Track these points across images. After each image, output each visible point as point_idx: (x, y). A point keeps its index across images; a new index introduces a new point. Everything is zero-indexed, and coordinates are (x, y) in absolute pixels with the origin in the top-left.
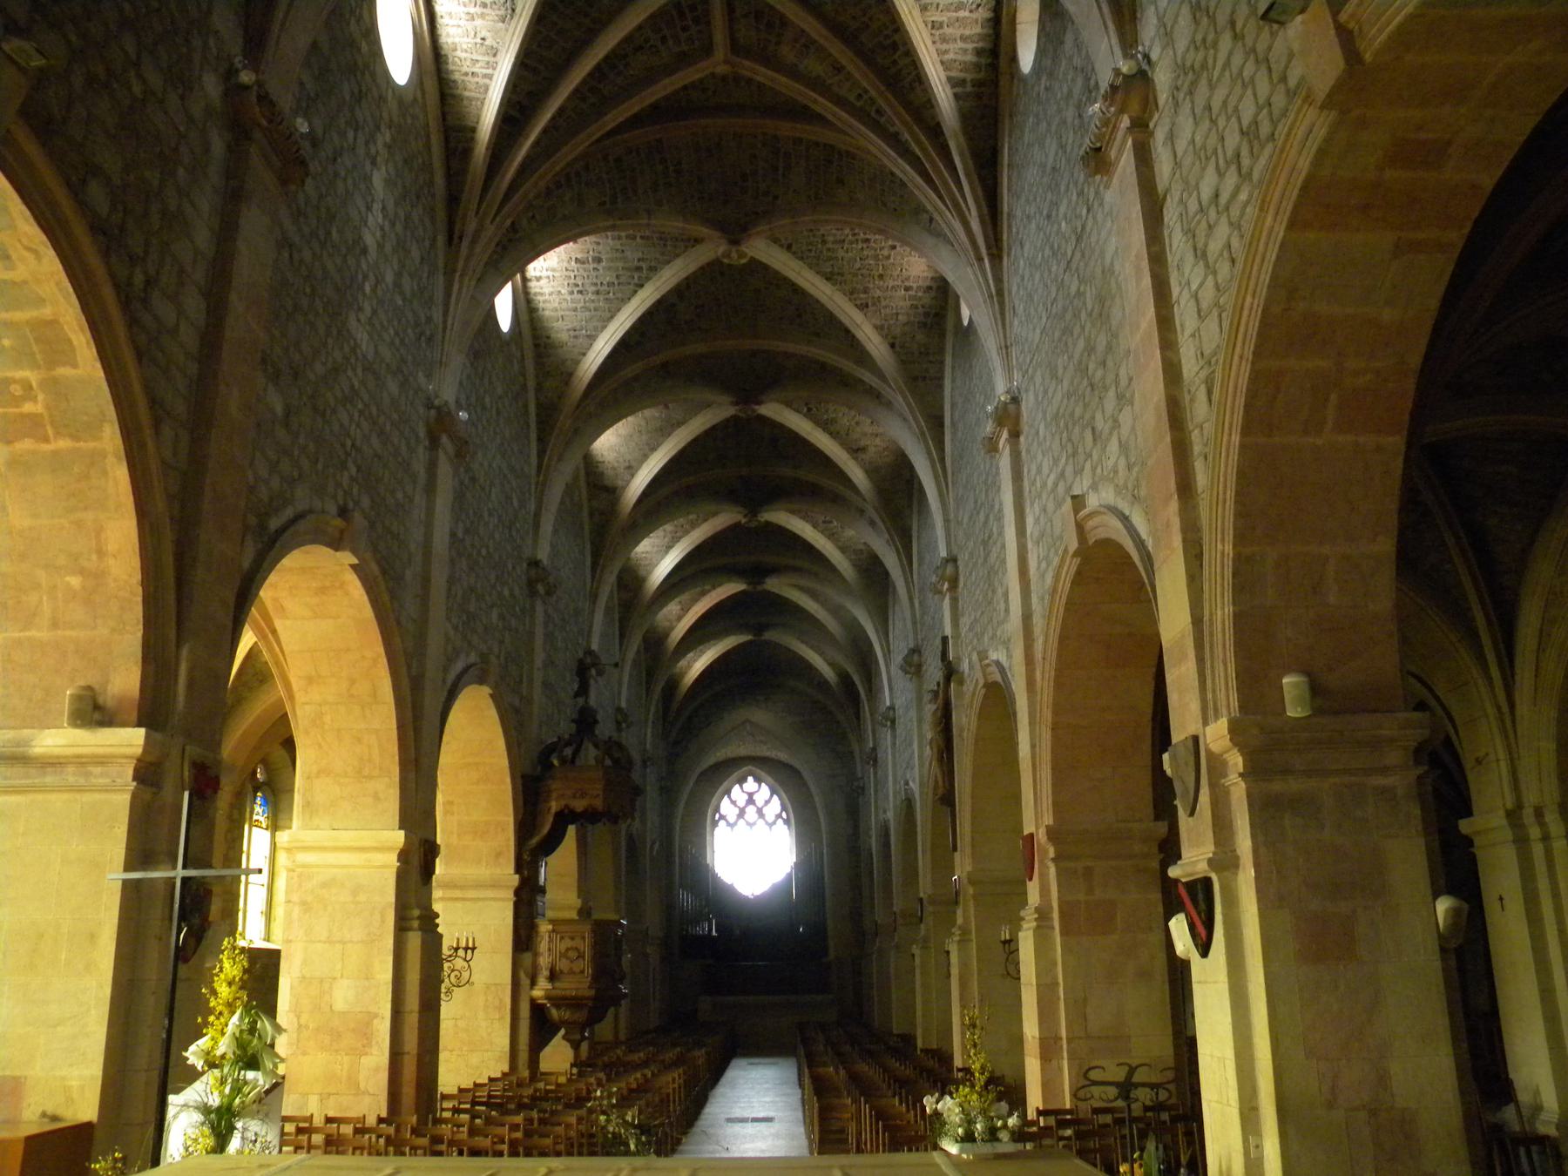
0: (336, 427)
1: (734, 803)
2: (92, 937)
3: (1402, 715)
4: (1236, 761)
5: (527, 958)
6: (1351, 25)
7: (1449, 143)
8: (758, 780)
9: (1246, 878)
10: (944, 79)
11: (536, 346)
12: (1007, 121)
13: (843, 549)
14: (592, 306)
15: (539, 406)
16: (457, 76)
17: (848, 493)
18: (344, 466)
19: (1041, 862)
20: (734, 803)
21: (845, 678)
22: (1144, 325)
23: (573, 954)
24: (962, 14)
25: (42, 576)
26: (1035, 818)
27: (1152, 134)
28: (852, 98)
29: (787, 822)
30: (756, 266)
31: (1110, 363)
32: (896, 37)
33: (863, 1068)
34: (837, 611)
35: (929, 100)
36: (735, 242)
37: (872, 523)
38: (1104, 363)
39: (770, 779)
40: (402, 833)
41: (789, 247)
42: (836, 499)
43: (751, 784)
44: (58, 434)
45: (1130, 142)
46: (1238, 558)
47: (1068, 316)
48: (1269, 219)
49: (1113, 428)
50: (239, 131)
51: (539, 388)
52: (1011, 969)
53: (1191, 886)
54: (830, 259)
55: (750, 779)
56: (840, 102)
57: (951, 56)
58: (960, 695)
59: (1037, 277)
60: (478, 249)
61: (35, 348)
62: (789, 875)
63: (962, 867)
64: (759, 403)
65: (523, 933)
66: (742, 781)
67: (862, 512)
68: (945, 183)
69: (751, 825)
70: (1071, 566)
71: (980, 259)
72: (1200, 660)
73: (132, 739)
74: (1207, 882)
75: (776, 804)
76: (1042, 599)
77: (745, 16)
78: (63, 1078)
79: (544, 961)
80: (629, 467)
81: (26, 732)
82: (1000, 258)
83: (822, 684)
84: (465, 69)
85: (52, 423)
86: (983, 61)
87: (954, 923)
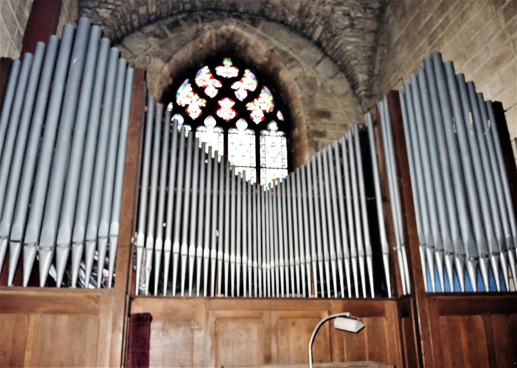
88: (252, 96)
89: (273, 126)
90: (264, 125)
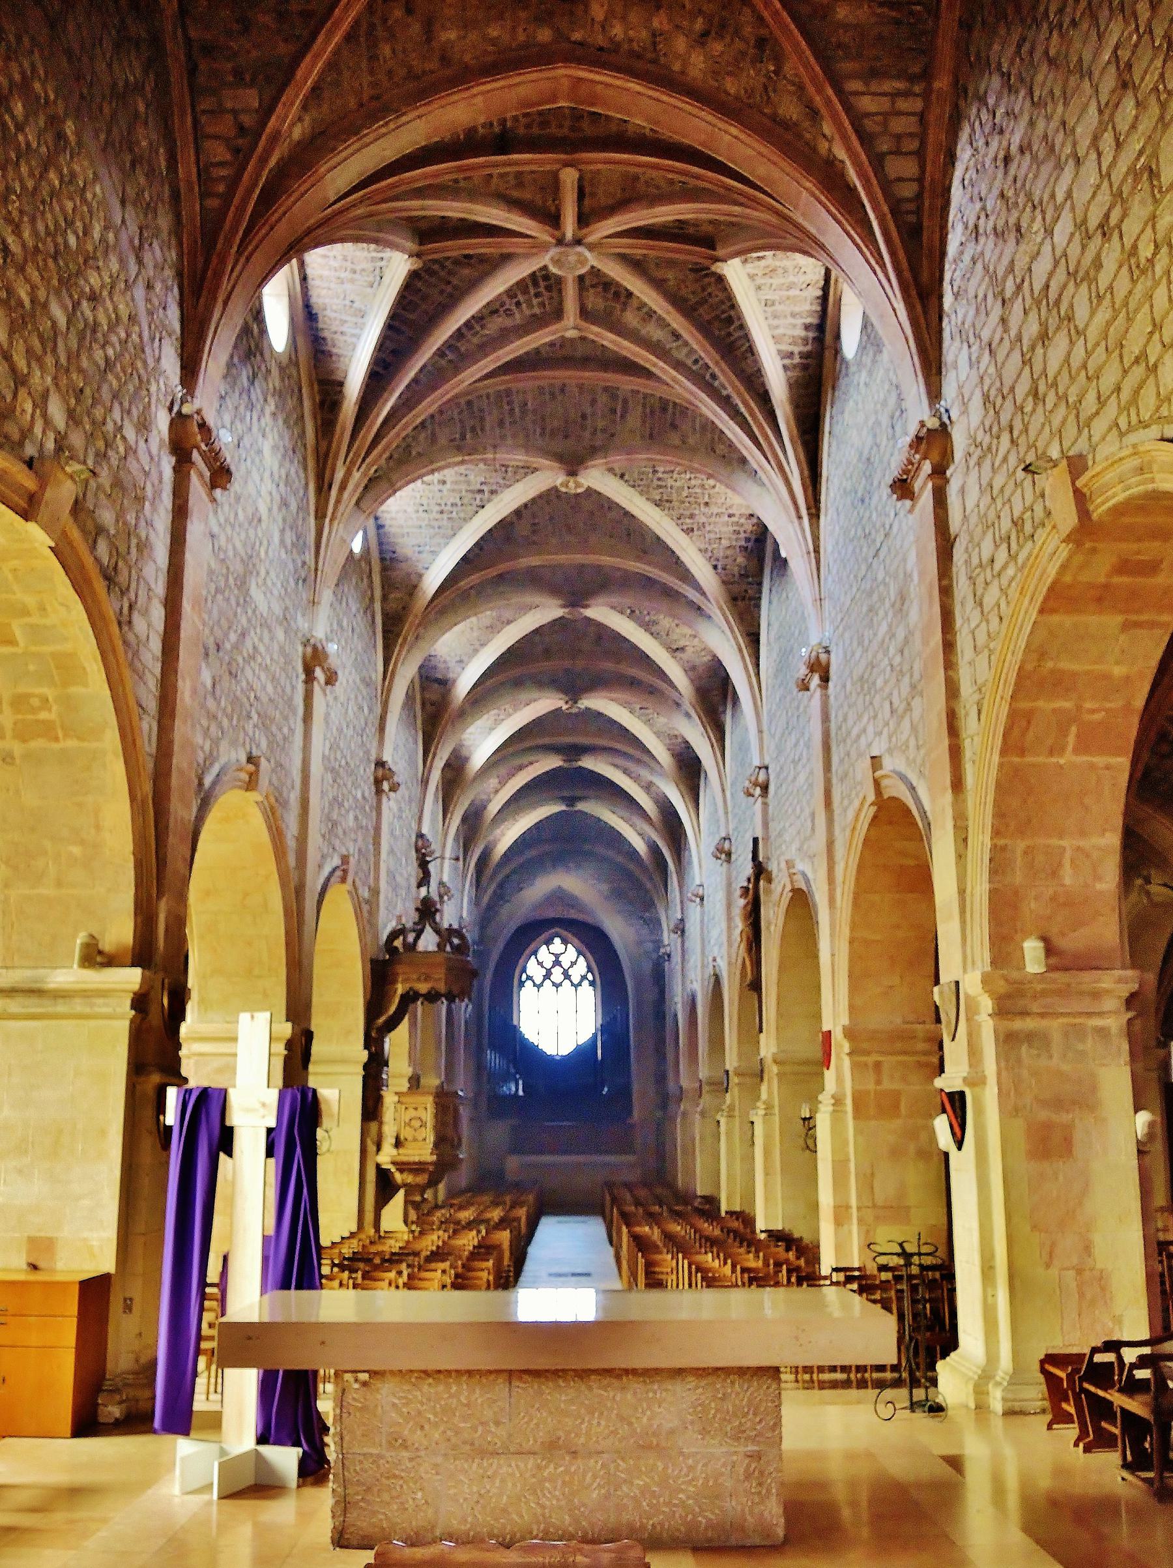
0: (244, 684)
1: (540, 964)
2: (103, 1133)
3: (1118, 973)
4: (986, 1004)
5: (373, 1126)
6: (1085, 490)
7: (1161, 561)
8: (565, 942)
9: (990, 1094)
10: (774, 353)
11: (382, 559)
12: (828, 408)
13: (658, 734)
14: (436, 524)
15: (385, 615)
16: (326, 334)
17: (663, 686)
18: (249, 717)
19: (838, 1056)
20: (540, 964)
21: (654, 849)
22: (932, 644)
23: (417, 1124)
24: (792, 293)
25: (48, 844)
26: (834, 1015)
27: (947, 481)
28: (689, 362)
29: (592, 983)
30: (590, 492)
31: (906, 652)
32: (732, 313)
33: (676, 1228)
34: (648, 787)
35: (759, 370)
36: (572, 473)
37: (688, 715)
38: (902, 652)
39: (576, 941)
40: (289, 1025)
41: (622, 476)
42: (652, 691)
43: (557, 945)
44: (66, 736)
45: (930, 485)
46: (994, 848)
47: (875, 597)
48: (1026, 602)
49: (905, 711)
50: (180, 450)
51: (385, 598)
52: (810, 1142)
53: (951, 1095)
54: (660, 487)
55: (557, 941)
56: (678, 365)
57: (780, 331)
58: (768, 892)
59: (850, 548)
60: (346, 495)
61: (55, 672)
62: (595, 1035)
63: (768, 1047)
64: (586, 606)
65: (371, 1103)
66: (548, 942)
67: (678, 705)
68: (771, 445)
69: (557, 986)
70: (869, 812)
71: (800, 517)
72: (963, 922)
73: (132, 977)
74: (962, 1094)
75: (581, 966)
76: (844, 830)
77: (593, 286)
78: (85, 1240)
79: (389, 1131)
80: (461, 661)
81: (42, 972)
82: (818, 517)
83: (633, 853)
84: (334, 328)
85: (62, 727)
86: (811, 335)
87: (758, 1098)
88: (573, 964)
89: (586, 983)
90: (580, 984)
